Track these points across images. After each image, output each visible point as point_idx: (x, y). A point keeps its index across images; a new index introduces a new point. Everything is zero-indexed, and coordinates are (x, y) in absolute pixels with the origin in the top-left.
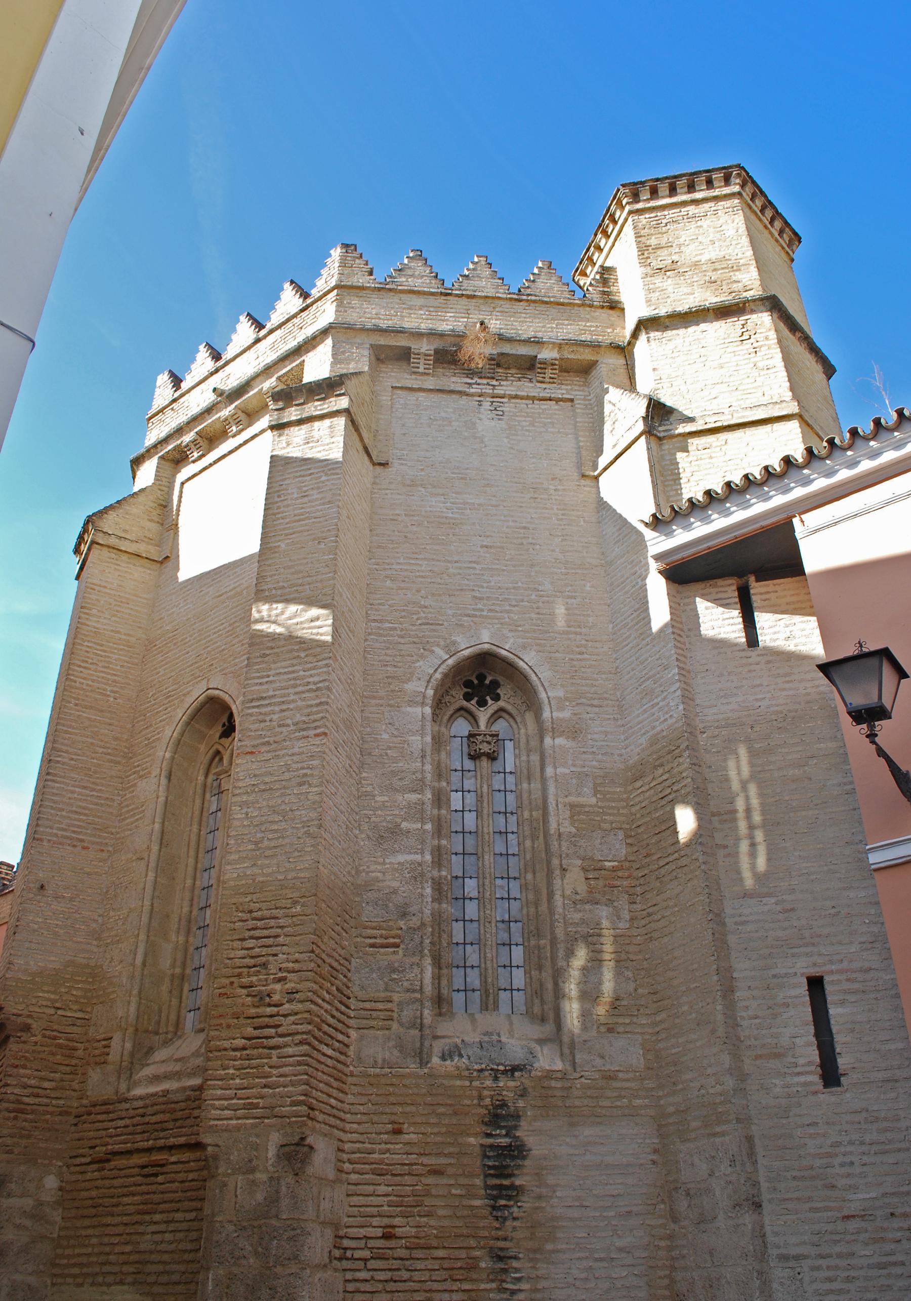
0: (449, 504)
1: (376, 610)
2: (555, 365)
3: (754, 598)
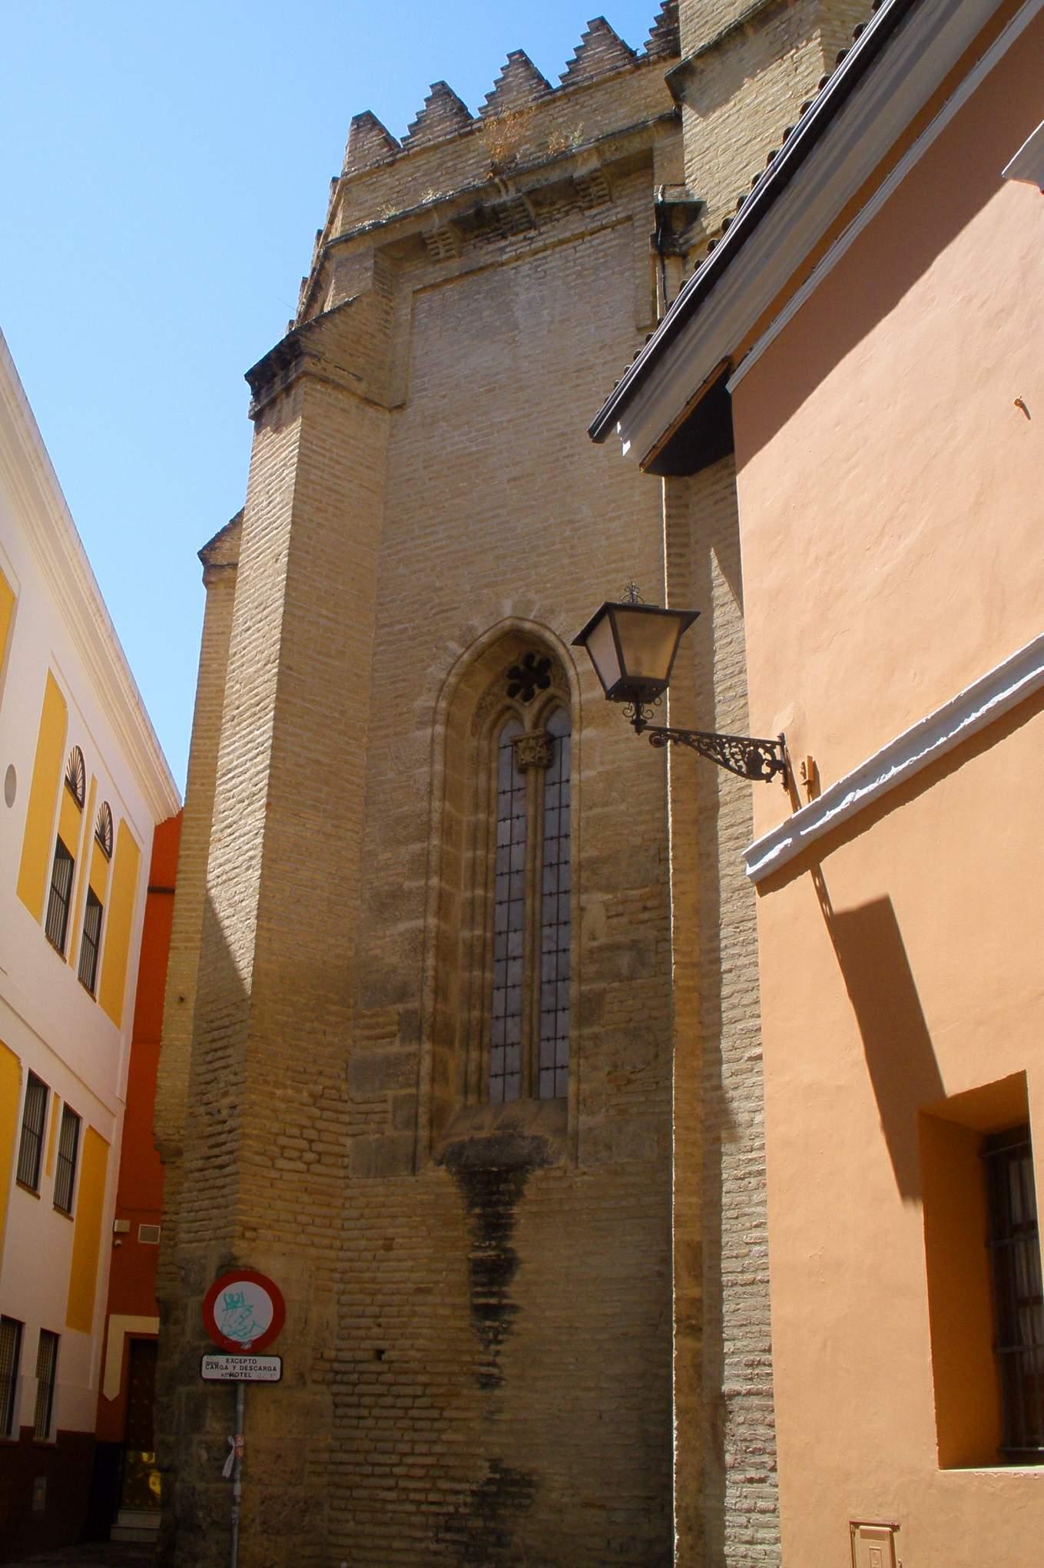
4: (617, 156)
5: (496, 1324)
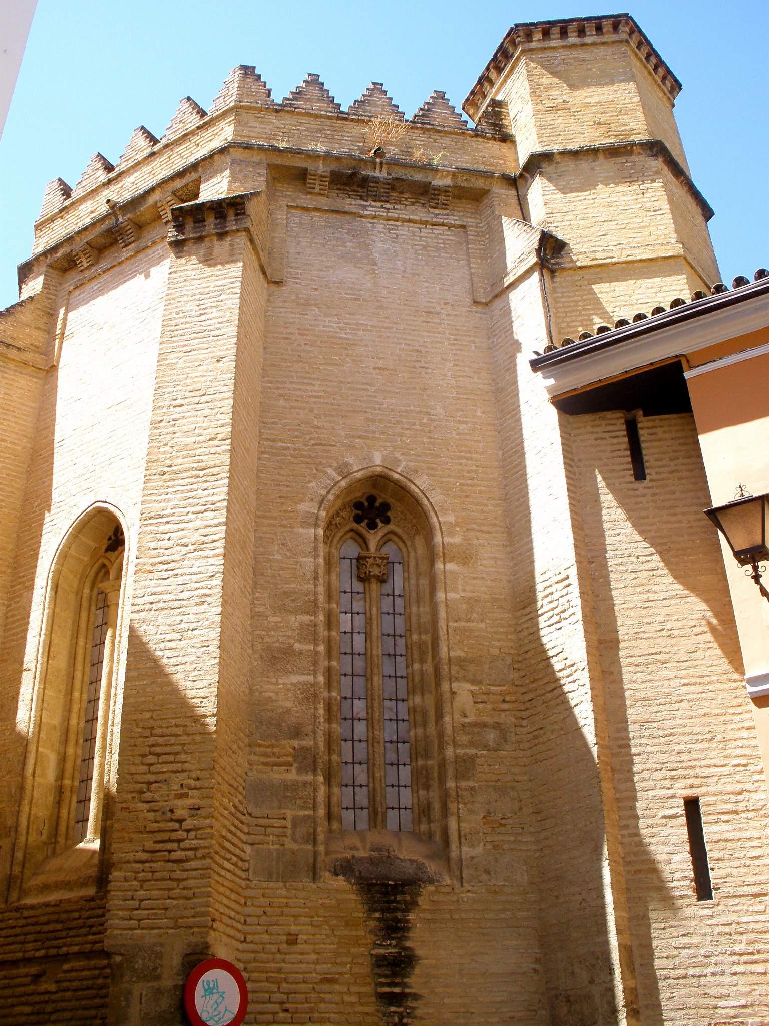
0: (342, 325)
1: (269, 429)
2: (448, 192)
3: (641, 432)
4: (465, 184)
5: (401, 1010)
